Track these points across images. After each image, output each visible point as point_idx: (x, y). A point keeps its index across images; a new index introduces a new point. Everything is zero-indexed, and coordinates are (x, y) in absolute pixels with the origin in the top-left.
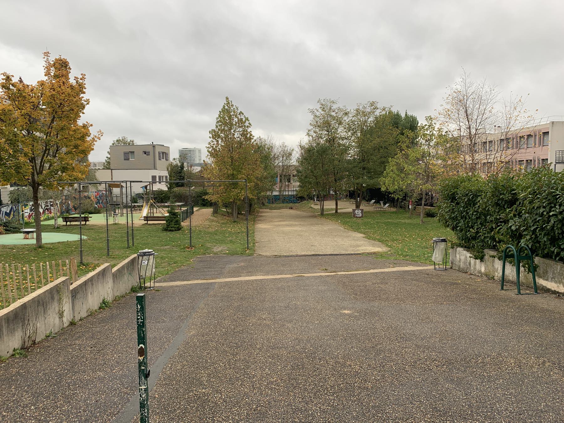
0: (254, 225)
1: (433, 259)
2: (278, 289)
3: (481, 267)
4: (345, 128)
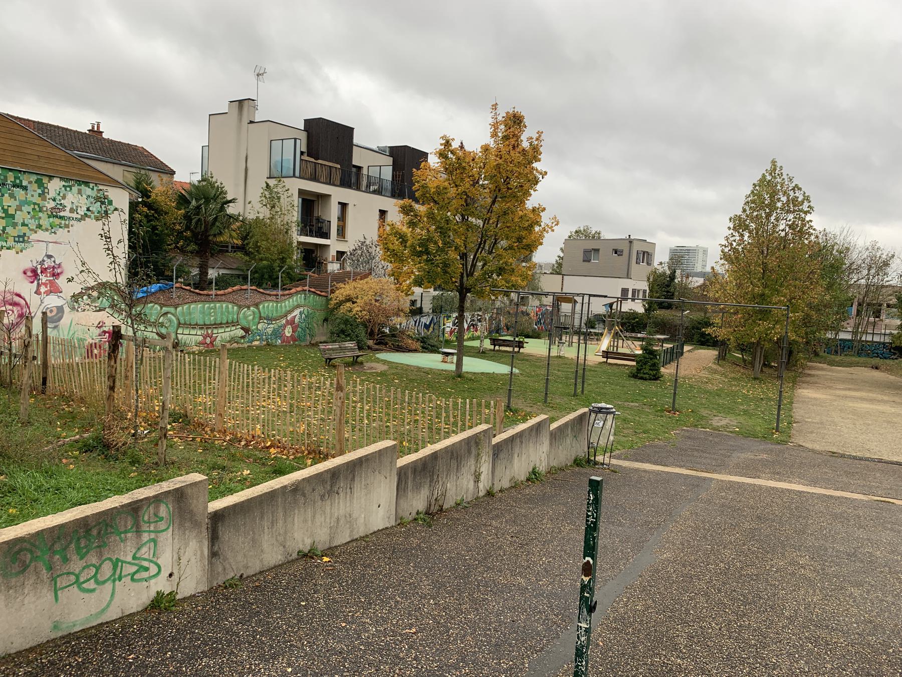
2: (835, 516)
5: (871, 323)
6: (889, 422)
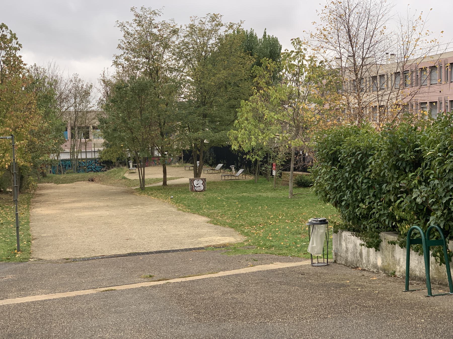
0: (28, 209)
1: (309, 250)
2: (73, 314)
3: (376, 259)
4: (174, 54)
5: (83, 143)
6: (105, 223)
